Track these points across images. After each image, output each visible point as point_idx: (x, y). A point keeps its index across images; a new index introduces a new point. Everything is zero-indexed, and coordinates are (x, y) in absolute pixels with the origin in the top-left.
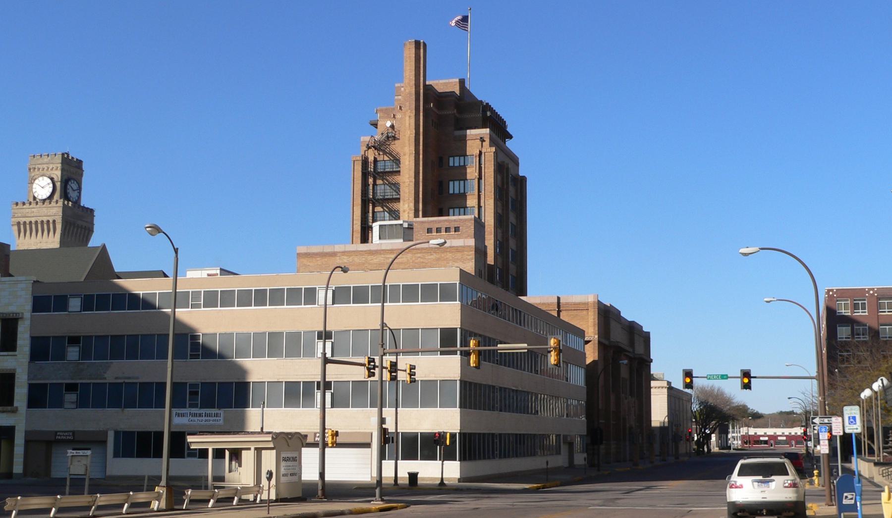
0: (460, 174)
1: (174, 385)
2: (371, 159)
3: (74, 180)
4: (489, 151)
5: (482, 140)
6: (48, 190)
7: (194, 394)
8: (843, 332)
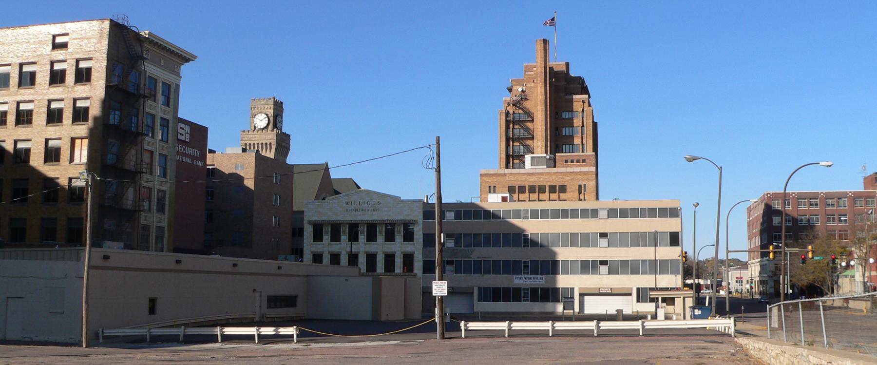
0: (570, 123)
2: (511, 112)
5: (583, 102)
6: (264, 123)
7: (526, 267)
8: (776, 220)
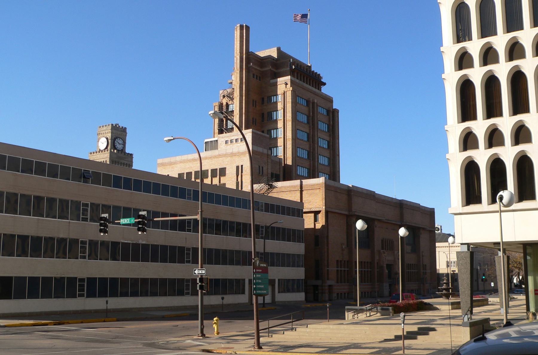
1: (204, 250)
2: (224, 104)
3: (120, 138)
5: (286, 84)
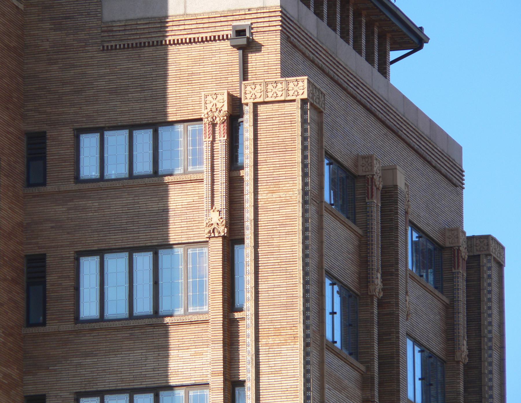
0: (138, 221)
4: (280, 98)
5: (246, 44)
